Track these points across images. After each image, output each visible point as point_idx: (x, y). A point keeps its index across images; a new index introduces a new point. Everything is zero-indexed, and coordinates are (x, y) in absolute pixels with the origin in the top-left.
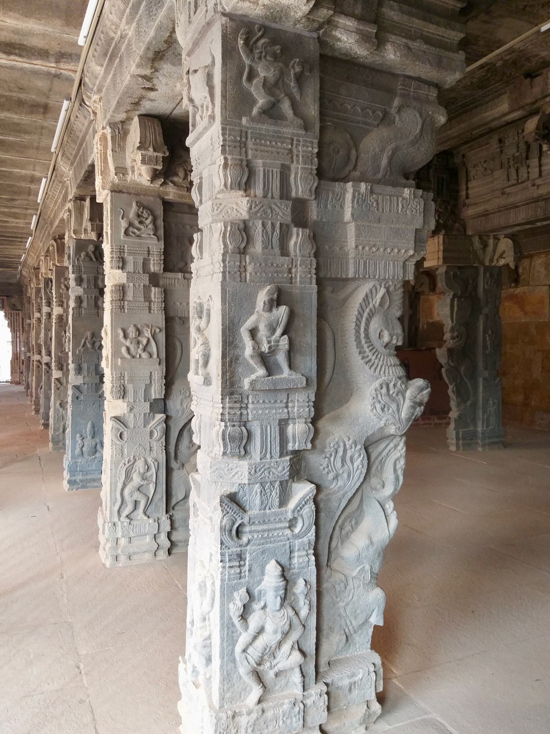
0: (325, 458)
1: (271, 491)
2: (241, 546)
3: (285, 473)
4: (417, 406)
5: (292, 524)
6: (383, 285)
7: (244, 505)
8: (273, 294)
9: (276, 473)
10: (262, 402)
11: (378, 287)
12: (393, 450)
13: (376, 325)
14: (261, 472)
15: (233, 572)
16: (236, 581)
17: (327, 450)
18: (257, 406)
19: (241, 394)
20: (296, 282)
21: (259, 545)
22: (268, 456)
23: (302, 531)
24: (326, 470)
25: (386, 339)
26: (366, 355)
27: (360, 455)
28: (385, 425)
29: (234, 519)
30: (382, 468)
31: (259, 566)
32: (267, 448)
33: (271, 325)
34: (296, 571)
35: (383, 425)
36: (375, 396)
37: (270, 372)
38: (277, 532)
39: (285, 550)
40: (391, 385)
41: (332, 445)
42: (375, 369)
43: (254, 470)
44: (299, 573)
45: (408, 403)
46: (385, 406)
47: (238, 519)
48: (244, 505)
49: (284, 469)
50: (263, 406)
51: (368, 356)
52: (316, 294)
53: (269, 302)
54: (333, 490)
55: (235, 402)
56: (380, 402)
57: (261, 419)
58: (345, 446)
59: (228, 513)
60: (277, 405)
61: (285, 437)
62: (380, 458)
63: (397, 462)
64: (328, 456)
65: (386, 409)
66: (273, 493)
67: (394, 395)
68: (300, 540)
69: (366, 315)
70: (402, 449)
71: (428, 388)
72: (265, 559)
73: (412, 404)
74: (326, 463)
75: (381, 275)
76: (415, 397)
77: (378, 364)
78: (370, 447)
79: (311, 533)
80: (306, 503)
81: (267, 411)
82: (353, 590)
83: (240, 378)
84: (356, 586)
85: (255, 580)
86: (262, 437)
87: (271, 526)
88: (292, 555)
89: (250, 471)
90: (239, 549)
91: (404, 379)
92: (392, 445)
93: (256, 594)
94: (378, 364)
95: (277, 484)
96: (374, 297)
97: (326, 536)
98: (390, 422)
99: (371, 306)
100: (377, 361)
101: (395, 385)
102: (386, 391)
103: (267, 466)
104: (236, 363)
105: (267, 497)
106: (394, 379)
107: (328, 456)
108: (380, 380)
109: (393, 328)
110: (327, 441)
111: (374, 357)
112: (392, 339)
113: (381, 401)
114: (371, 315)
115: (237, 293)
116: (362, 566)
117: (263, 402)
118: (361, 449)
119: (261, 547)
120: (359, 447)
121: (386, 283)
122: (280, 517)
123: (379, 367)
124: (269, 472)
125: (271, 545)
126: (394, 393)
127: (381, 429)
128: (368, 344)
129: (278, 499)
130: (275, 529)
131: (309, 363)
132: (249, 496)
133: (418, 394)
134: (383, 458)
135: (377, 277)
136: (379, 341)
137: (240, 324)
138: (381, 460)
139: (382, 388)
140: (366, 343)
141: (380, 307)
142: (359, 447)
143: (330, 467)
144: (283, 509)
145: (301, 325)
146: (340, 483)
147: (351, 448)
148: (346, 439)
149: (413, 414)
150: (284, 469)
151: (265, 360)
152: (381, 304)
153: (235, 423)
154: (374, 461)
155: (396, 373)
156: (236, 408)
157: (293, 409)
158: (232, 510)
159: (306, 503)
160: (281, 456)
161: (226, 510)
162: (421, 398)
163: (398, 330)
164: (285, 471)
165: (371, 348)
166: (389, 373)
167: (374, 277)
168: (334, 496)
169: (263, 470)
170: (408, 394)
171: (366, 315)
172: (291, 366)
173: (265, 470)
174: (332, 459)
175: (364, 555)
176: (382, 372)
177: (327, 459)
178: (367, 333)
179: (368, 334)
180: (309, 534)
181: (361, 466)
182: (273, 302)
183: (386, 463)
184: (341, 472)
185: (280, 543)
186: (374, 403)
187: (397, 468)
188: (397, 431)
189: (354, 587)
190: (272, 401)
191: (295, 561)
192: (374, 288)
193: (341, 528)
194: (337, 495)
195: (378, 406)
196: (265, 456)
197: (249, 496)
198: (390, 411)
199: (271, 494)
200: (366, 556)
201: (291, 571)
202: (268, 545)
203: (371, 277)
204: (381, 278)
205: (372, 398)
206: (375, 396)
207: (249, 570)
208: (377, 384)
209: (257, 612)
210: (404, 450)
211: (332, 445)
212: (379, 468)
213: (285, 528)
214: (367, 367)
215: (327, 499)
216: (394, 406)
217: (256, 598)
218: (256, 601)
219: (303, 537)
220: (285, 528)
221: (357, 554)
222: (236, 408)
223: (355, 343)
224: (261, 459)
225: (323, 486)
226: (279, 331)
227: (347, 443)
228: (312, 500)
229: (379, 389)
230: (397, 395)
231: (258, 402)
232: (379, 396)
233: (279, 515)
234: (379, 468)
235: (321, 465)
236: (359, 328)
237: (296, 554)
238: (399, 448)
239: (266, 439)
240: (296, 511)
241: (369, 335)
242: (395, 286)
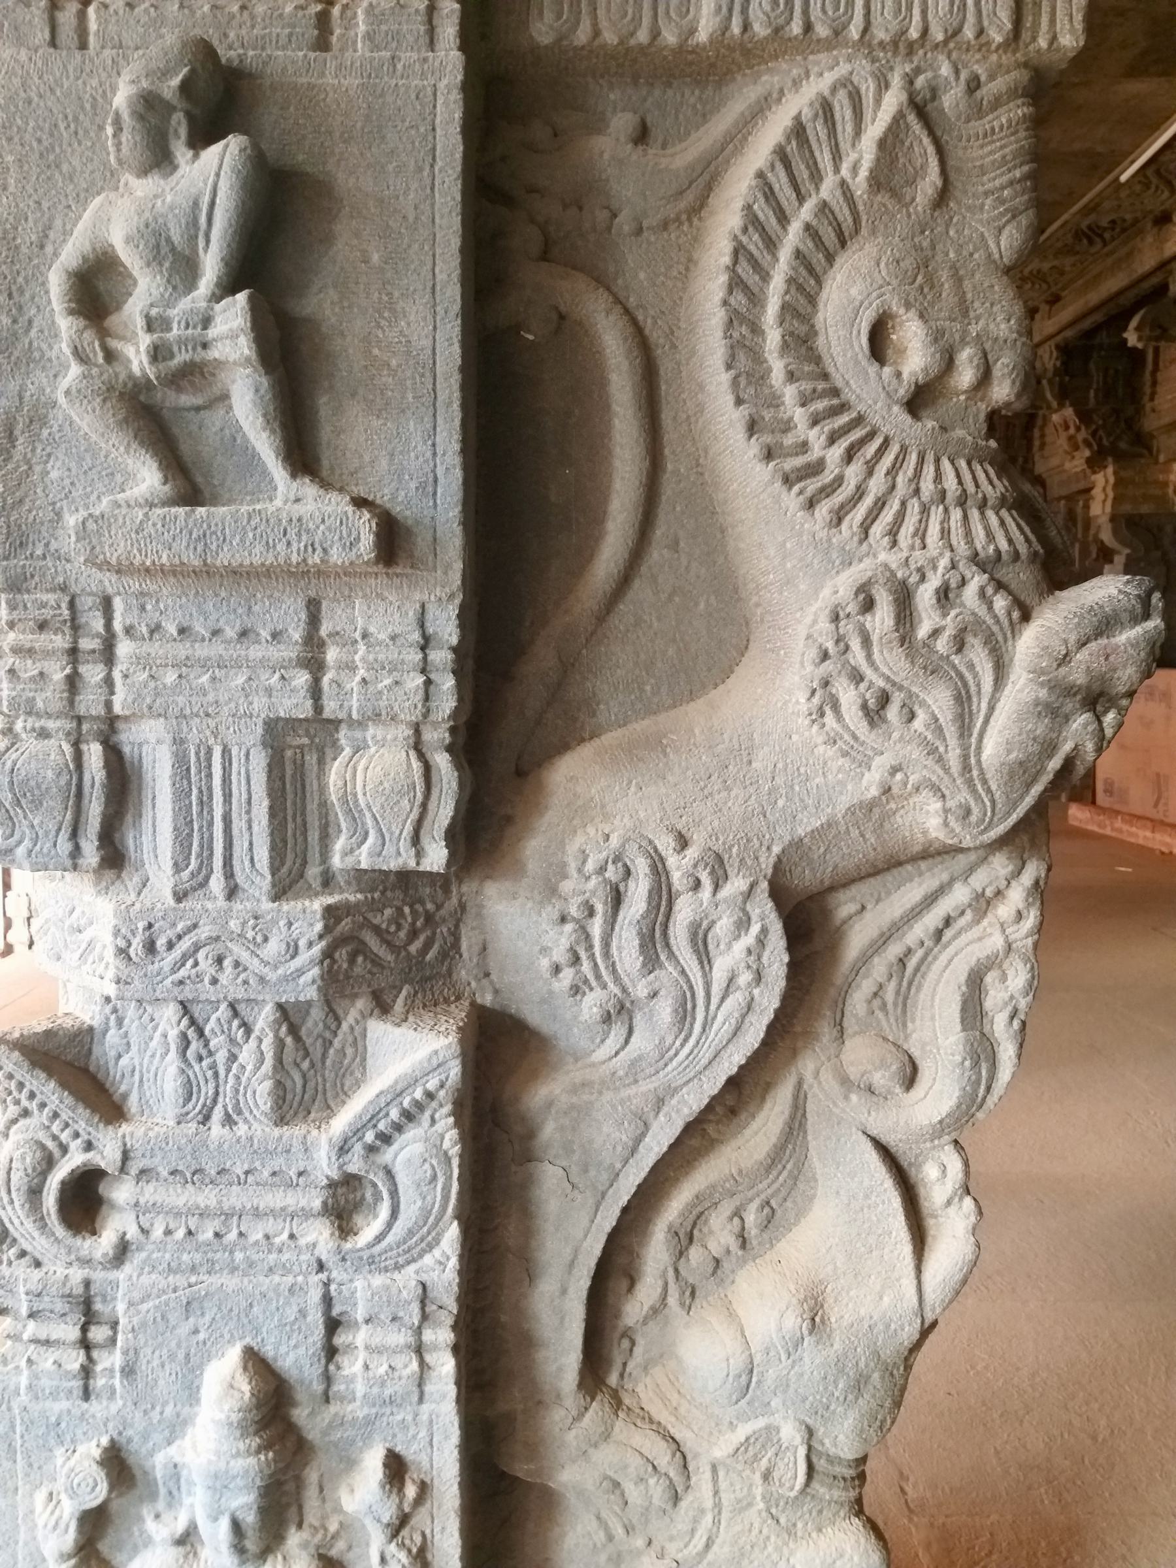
0: (563, 919)
1: (232, 1041)
2: (86, 1262)
3: (300, 972)
4: (1069, 706)
5: (344, 1204)
6: (896, 80)
7: (123, 1088)
8: (165, 74)
9: (254, 964)
10: (172, 630)
11: (868, 88)
12: (969, 916)
13: (849, 293)
14: (177, 953)
15: (48, 1365)
16: (64, 1405)
17: (567, 886)
18: (155, 648)
19: (64, 588)
20: (348, 44)
21: (170, 1270)
22: (217, 883)
23: (390, 1239)
24: (568, 975)
25: (915, 356)
26: (789, 440)
27: (743, 924)
28: (887, 790)
29: (50, 1144)
30: (904, 1000)
31: (172, 1357)
32: (207, 846)
33: (157, 234)
34: (357, 1410)
35: (874, 792)
36: (830, 645)
37: (189, 485)
38: (270, 1225)
39: (303, 1313)
40: (925, 595)
41: (590, 866)
42: (839, 516)
43: (144, 946)
44: (369, 1422)
45: (1021, 688)
46: (884, 699)
47: (75, 1145)
48: (123, 1088)
49: (293, 950)
50: (183, 654)
51: (804, 447)
52: (456, 96)
53: (140, 117)
54: (605, 1070)
55: (42, 626)
56: (857, 677)
57: (173, 711)
58: (659, 869)
59: (26, 1113)
60: (255, 652)
61: (312, 806)
62: (894, 950)
63: (988, 979)
64: (574, 911)
65: (893, 712)
66: (246, 1055)
67: (942, 645)
68: (378, 1280)
69: (793, 237)
70: (1019, 916)
71: (1146, 616)
72: (202, 1336)
73: (1043, 693)
74: (564, 943)
75: (877, 19)
76: (1065, 659)
77: (860, 493)
78: (842, 896)
79: (437, 1252)
80: (408, 1116)
81: (205, 678)
82: (708, 1518)
83: (59, 514)
84: (726, 1498)
85: (155, 1416)
86: (181, 795)
87: (236, 1198)
88: (340, 1340)
89: (122, 943)
90: (77, 1275)
91: (1022, 577)
92: (960, 895)
93: (159, 1474)
94: (860, 493)
95: (264, 1018)
96: (844, 145)
97: (572, 1265)
98: (913, 779)
99: (828, 189)
100: (853, 473)
101: (944, 596)
102: (890, 622)
103: (204, 932)
104: (34, 439)
105: (213, 1067)
106: (944, 562)
107: (574, 911)
108: (867, 563)
109: (964, 308)
110: (572, 848)
111: (836, 453)
112: (949, 364)
113: (869, 673)
114: (829, 236)
115: (29, 102)
116: (761, 1423)
117: (182, 631)
118: (749, 894)
119: (179, 1280)
120: (736, 885)
121: (918, 71)
122: (278, 1163)
123: (868, 501)
124: (219, 960)
125: (231, 1282)
126: (936, 633)
127: (874, 810)
128: (806, 386)
129: (268, 1084)
130: (257, 1214)
131: (418, 454)
132: (142, 1052)
133: (1082, 644)
134: (909, 952)
135: (854, 32)
136: (873, 368)
137: (49, 249)
138: (902, 962)
139: (868, 605)
140: (791, 377)
141: (882, 198)
142: (736, 885)
143: (586, 967)
144: (294, 1132)
145: (375, 258)
146: (641, 1042)
147: (697, 885)
148: (666, 844)
149: (1050, 748)
150: (293, 950)
151: (157, 417)
152: (889, 174)
153: (51, 725)
154: (865, 959)
155: (968, 534)
156: (48, 654)
157: (344, 676)
158: (43, 1105)
159: (408, 1116)
160: (280, 892)
161: (17, 1102)
162: (1100, 665)
163: (998, 318)
164: (298, 962)
165: (820, 405)
166: (921, 533)
167: (838, 32)
168: (608, 1096)
169: (185, 944)
170: (1028, 645)
171: (793, 237)
172: (303, 455)
173: (197, 948)
174: (596, 928)
175: (771, 1374)
176: (877, 529)
177: (569, 927)
178: (802, 329)
179: (813, 332)
180: (428, 1259)
181: (745, 978)
182: (166, 119)
183: (932, 976)
184: (641, 990)
185: (276, 1279)
186: (826, 684)
187: (988, 1004)
188: (953, 823)
189: (718, 1506)
190: (230, 633)
191: (351, 1367)
192: (842, 94)
193: (685, 1238)
194: (625, 1093)
195: (848, 697)
196: (204, 884)
197: (142, 1052)
198: (918, 724)
199: (233, 1058)
200: (783, 1385)
201: (333, 1408)
202: (215, 1281)
203: (822, 31)
204: (880, 34)
205: (813, 653)
206: (830, 645)
207: (123, 1371)
208: (841, 586)
209: (159, 1550)
210: (1031, 920)
211: (590, 866)
212: (889, 995)
213: (306, 1214)
214: (792, 500)
215: (573, 1107)
216: (938, 700)
217: (162, 1491)
218: (161, 1505)
219: (398, 1267)
220: (306, 1214)
221: (738, 1363)
222: (48, 654)
223: (725, 377)
224: (180, 897)
225: (562, 1044)
226: (211, 265)
227: (672, 861)
228: (448, 1108)
229: (852, 608)
230: (960, 644)
231: (155, 629)
232: (855, 644)
233: (272, 1153)
234: (889, 995)
235: (544, 950)
236: (756, 299)
237: (359, 1337)
238: (1004, 911)
239: (205, 802)
240: (358, 1148)
241: (821, 341)
242: (974, 84)
